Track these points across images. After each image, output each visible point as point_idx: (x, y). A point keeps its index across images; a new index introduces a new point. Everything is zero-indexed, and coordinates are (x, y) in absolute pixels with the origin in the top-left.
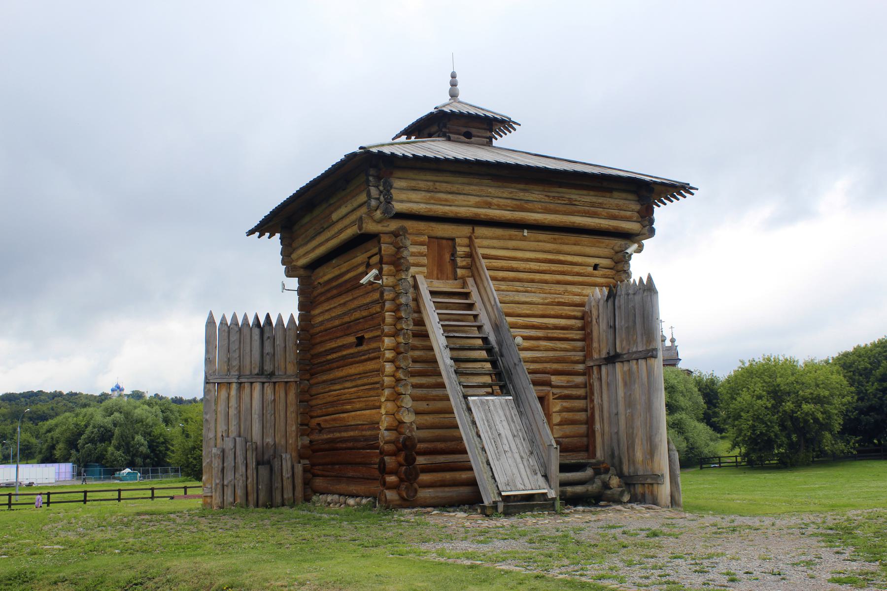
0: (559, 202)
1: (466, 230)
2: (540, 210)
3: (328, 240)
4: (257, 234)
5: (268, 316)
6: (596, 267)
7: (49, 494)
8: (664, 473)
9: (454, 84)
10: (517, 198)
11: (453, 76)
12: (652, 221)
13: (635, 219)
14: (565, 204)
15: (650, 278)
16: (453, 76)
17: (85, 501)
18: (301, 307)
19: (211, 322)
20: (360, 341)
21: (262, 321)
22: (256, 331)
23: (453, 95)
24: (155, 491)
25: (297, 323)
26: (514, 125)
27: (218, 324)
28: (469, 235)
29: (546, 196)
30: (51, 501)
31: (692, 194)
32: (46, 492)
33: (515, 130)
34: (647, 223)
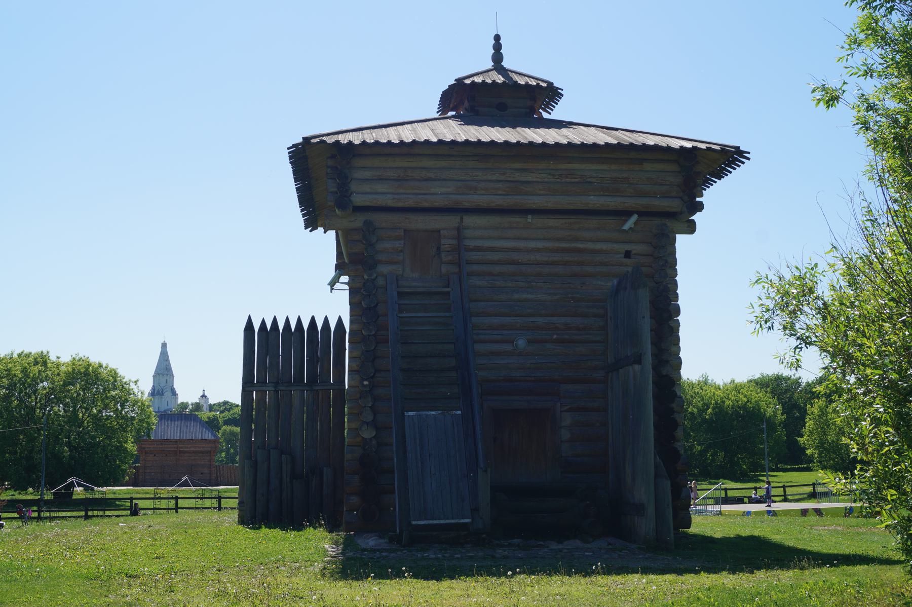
0: (568, 180)
1: (451, 221)
2: (542, 192)
5: (275, 320)
6: (628, 254)
7: (784, 487)
8: (844, 506)
9: (497, 46)
10: (512, 179)
11: (497, 38)
14: (577, 183)
16: (497, 38)
17: (220, 508)
23: (497, 57)
24: (728, 491)
29: (550, 174)
30: (179, 506)
32: (781, 485)
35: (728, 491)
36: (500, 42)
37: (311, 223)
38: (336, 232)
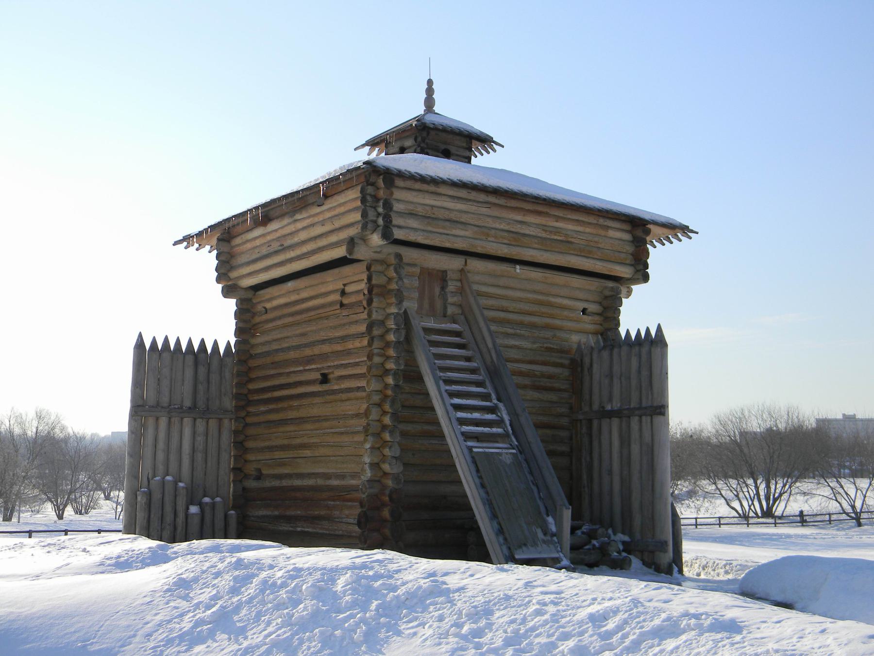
1: (453, 263)
3: (291, 260)
4: (185, 244)
9: (430, 91)
11: (430, 82)
12: (646, 266)
13: (628, 262)
15: (659, 329)
16: (430, 82)
18: (239, 332)
19: (140, 344)
20: (325, 379)
21: (196, 347)
22: (190, 359)
23: (429, 102)
24: (698, 519)
25: (234, 351)
26: (494, 145)
27: (148, 346)
28: (461, 267)
31: (690, 238)
33: (494, 150)
34: (641, 267)
35: (698, 519)
36: (426, 96)
37: (112, 433)
38: (238, 315)
